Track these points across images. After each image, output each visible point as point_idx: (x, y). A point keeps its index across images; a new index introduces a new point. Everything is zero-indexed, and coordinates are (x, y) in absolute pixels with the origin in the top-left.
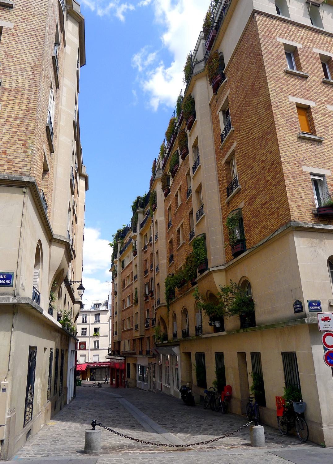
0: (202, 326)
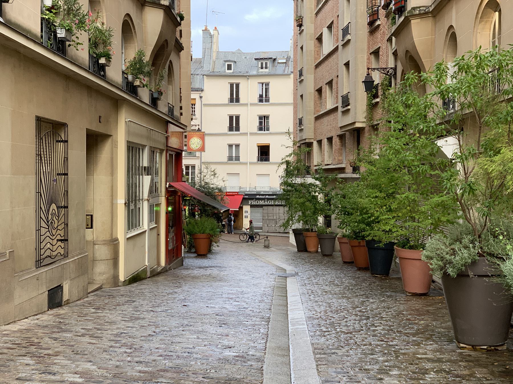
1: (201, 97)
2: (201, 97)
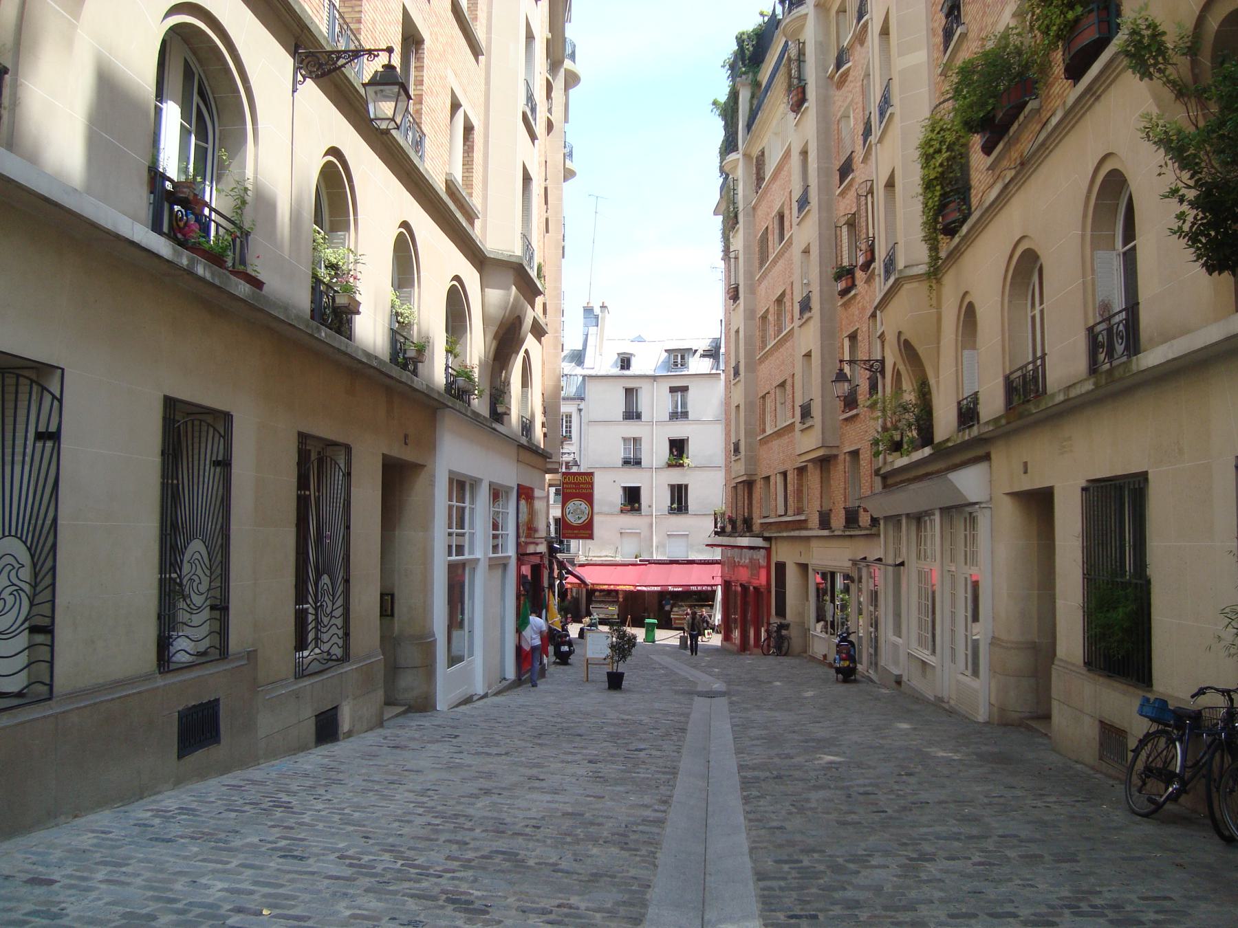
0: (1132, 307)
1: (580, 410)
2: (580, 410)
